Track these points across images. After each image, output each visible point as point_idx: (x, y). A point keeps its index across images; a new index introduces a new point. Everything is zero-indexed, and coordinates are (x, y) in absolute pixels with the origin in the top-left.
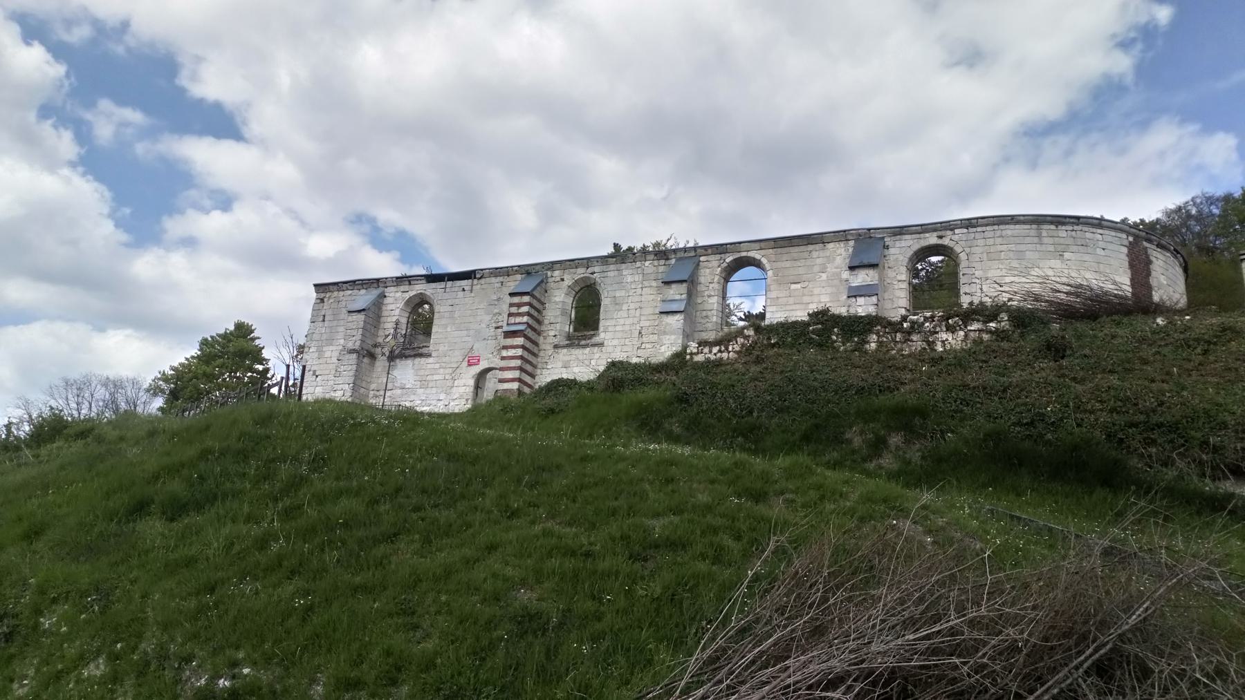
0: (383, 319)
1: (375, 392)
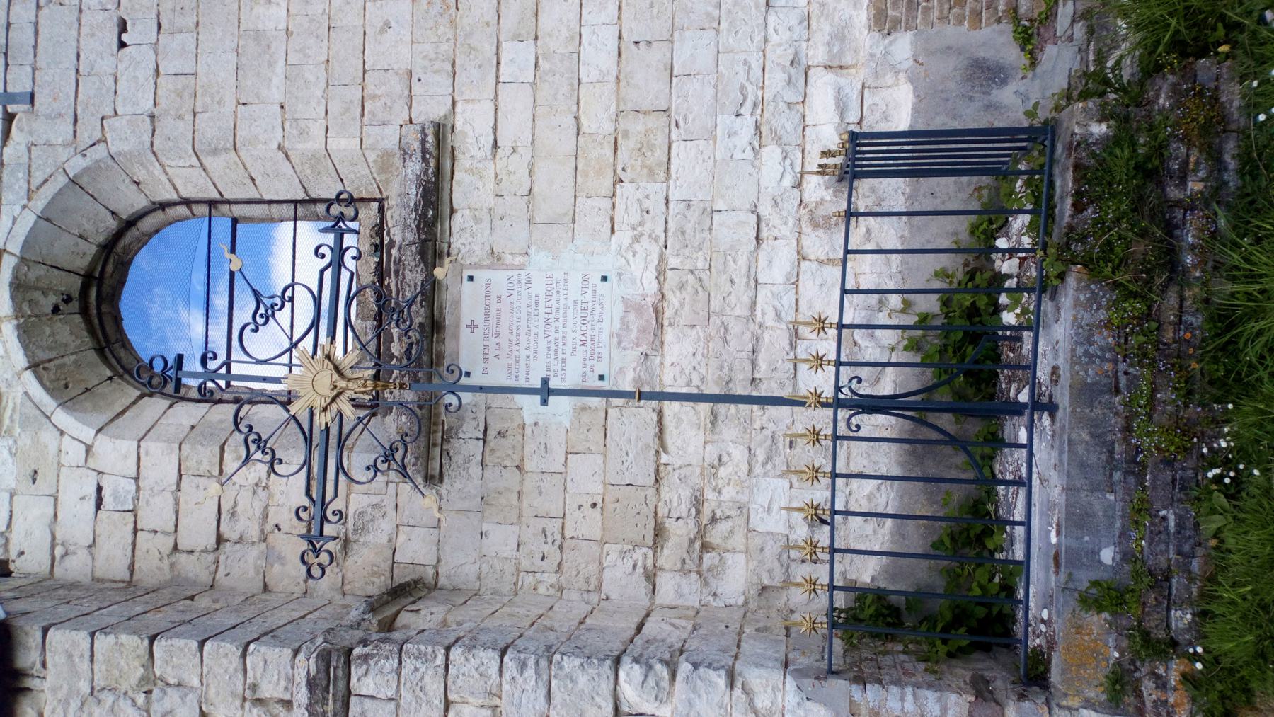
0: (151, 567)
1: (670, 555)
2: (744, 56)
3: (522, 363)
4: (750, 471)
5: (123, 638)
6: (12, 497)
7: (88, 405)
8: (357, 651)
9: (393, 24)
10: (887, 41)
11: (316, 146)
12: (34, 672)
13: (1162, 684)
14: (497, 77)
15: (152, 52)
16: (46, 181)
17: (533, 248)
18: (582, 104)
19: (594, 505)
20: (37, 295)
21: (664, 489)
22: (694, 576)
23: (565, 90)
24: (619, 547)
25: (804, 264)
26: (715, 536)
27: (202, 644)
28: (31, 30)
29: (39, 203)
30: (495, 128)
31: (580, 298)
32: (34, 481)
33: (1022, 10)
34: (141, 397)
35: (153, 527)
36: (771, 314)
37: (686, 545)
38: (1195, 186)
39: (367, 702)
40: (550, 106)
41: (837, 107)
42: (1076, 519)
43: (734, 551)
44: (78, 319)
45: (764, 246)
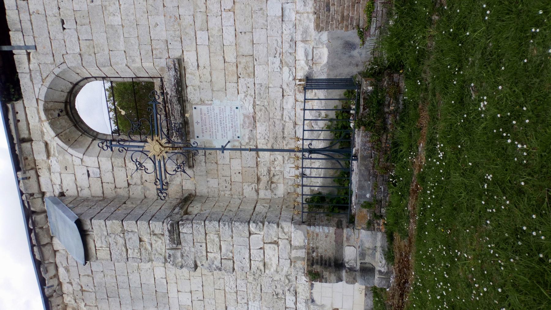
0: (109, 191)
1: (262, 185)
2: (276, 38)
3: (214, 133)
4: (284, 162)
5: (114, 221)
6: (60, 174)
7: (78, 146)
8: (180, 223)
9: (158, 24)
10: (320, 34)
11: (139, 65)
12: (90, 230)
13: (379, 225)
14: (196, 43)
15: (75, 32)
16: (48, 76)
17: (214, 99)
18: (225, 52)
19: (239, 173)
20: (52, 112)
21: (259, 168)
22: (269, 190)
23: (219, 48)
24: (247, 184)
25: (297, 103)
26: (274, 180)
27: (137, 222)
28: (29, 23)
29: (47, 83)
30: (197, 60)
31: (230, 114)
32: (66, 170)
33: (361, 25)
34: (93, 140)
35: (107, 182)
36: (288, 118)
37: (266, 182)
38: (392, 108)
39: (185, 235)
40: (215, 53)
41: (305, 55)
42: (361, 187)
43: (280, 183)
44: (66, 117)
45: (285, 98)
